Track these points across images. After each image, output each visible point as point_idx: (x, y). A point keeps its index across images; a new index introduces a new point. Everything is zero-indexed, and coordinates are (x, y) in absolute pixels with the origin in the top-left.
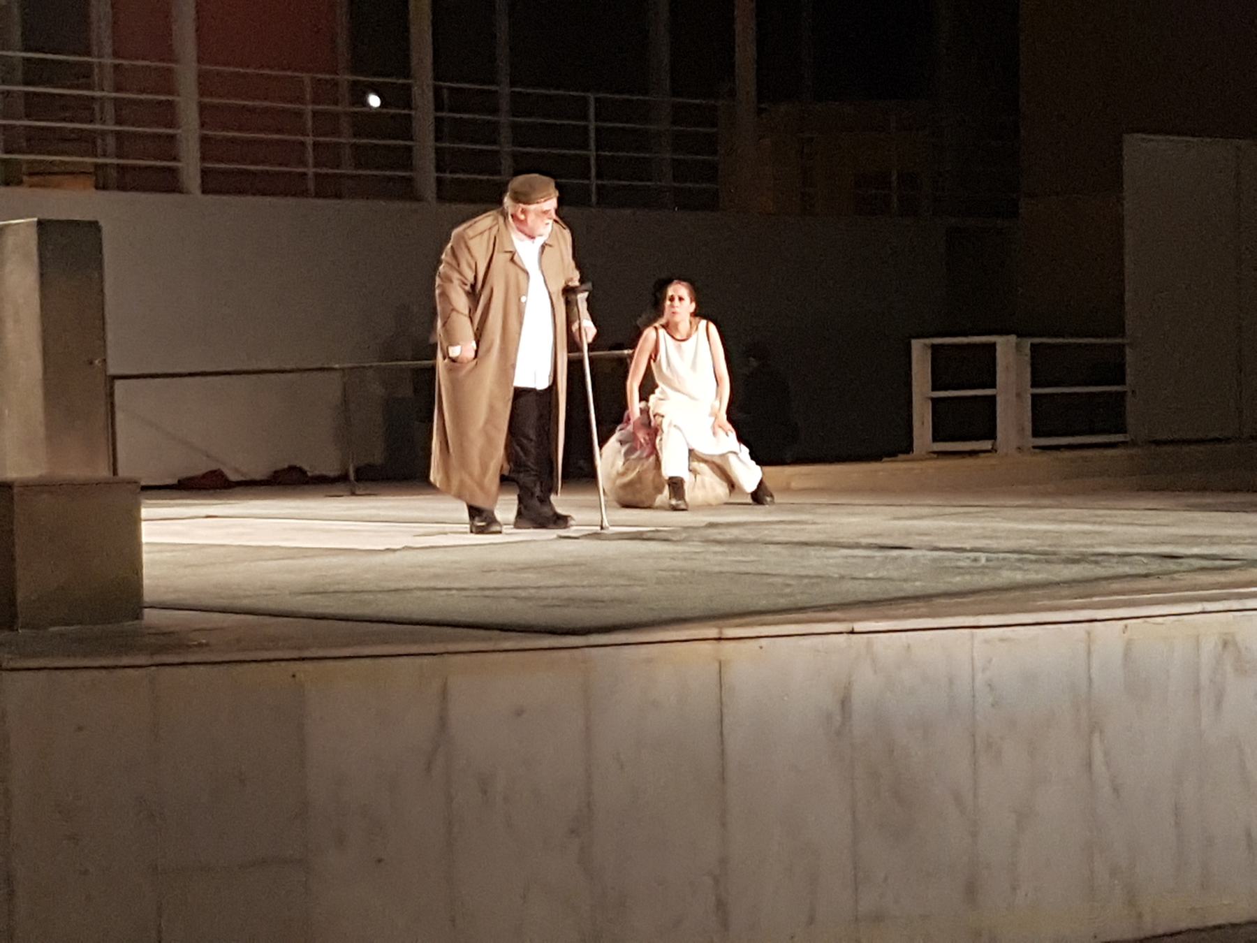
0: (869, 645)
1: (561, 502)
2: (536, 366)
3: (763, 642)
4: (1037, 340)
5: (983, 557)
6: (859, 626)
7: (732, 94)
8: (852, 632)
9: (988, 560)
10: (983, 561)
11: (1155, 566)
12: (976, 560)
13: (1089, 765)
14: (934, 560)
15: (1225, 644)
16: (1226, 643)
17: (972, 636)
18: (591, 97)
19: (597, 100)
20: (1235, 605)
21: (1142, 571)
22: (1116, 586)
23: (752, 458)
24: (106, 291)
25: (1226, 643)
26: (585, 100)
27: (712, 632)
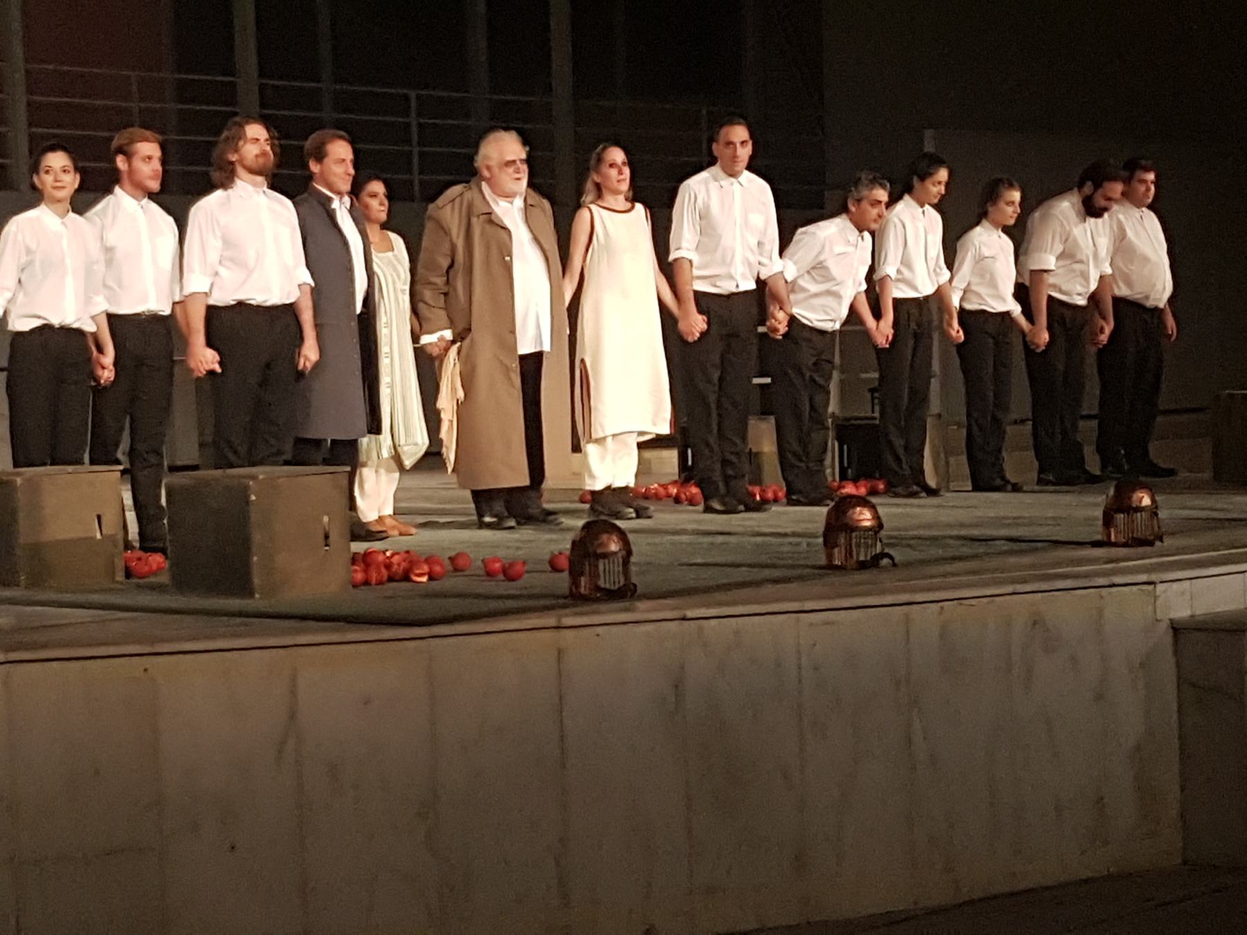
0: (701, 629)
1: (382, 471)
2: (836, 550)
3: (600, 630)
4: (307, 317)
5: (804, 541)
6: (690, 614)
7: (549, 89)
8: (684, 619)
9: (808, 545)
10: (805, 545)
11: (966, 550)
12: (798, 544)
13: (909, 741)
14: (758, 545)
15: (1035, 623)
16: (1037, 622)
17: (798, 620)
18: (413, 95)
19: (418, 97)
20: (1044, 586)
21: (950, 553)
22: (934, 570)
23: (240, 304)
24: (961, 375)
25: (1037, 622)
26: (406, 98)
27: (551, 621)
